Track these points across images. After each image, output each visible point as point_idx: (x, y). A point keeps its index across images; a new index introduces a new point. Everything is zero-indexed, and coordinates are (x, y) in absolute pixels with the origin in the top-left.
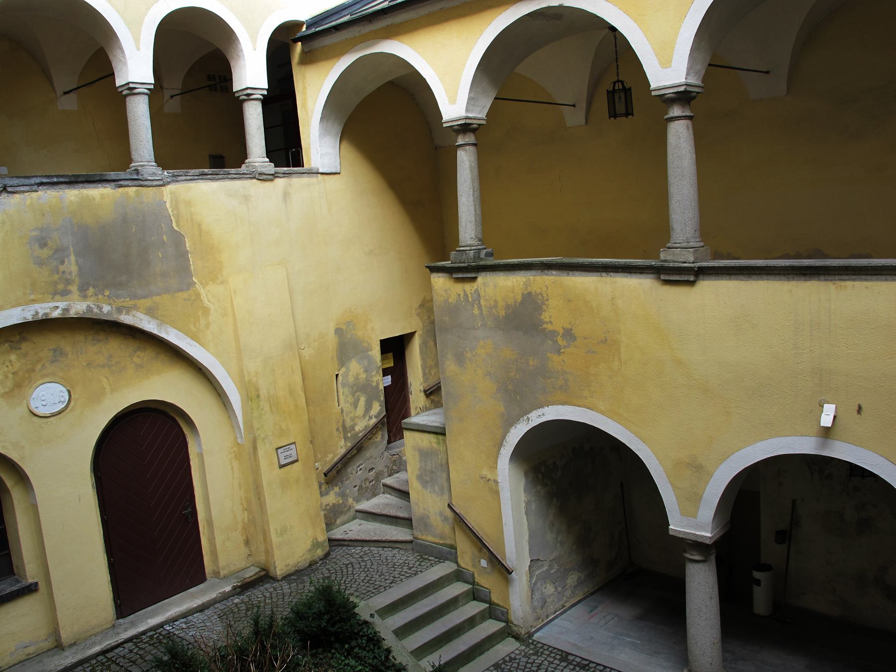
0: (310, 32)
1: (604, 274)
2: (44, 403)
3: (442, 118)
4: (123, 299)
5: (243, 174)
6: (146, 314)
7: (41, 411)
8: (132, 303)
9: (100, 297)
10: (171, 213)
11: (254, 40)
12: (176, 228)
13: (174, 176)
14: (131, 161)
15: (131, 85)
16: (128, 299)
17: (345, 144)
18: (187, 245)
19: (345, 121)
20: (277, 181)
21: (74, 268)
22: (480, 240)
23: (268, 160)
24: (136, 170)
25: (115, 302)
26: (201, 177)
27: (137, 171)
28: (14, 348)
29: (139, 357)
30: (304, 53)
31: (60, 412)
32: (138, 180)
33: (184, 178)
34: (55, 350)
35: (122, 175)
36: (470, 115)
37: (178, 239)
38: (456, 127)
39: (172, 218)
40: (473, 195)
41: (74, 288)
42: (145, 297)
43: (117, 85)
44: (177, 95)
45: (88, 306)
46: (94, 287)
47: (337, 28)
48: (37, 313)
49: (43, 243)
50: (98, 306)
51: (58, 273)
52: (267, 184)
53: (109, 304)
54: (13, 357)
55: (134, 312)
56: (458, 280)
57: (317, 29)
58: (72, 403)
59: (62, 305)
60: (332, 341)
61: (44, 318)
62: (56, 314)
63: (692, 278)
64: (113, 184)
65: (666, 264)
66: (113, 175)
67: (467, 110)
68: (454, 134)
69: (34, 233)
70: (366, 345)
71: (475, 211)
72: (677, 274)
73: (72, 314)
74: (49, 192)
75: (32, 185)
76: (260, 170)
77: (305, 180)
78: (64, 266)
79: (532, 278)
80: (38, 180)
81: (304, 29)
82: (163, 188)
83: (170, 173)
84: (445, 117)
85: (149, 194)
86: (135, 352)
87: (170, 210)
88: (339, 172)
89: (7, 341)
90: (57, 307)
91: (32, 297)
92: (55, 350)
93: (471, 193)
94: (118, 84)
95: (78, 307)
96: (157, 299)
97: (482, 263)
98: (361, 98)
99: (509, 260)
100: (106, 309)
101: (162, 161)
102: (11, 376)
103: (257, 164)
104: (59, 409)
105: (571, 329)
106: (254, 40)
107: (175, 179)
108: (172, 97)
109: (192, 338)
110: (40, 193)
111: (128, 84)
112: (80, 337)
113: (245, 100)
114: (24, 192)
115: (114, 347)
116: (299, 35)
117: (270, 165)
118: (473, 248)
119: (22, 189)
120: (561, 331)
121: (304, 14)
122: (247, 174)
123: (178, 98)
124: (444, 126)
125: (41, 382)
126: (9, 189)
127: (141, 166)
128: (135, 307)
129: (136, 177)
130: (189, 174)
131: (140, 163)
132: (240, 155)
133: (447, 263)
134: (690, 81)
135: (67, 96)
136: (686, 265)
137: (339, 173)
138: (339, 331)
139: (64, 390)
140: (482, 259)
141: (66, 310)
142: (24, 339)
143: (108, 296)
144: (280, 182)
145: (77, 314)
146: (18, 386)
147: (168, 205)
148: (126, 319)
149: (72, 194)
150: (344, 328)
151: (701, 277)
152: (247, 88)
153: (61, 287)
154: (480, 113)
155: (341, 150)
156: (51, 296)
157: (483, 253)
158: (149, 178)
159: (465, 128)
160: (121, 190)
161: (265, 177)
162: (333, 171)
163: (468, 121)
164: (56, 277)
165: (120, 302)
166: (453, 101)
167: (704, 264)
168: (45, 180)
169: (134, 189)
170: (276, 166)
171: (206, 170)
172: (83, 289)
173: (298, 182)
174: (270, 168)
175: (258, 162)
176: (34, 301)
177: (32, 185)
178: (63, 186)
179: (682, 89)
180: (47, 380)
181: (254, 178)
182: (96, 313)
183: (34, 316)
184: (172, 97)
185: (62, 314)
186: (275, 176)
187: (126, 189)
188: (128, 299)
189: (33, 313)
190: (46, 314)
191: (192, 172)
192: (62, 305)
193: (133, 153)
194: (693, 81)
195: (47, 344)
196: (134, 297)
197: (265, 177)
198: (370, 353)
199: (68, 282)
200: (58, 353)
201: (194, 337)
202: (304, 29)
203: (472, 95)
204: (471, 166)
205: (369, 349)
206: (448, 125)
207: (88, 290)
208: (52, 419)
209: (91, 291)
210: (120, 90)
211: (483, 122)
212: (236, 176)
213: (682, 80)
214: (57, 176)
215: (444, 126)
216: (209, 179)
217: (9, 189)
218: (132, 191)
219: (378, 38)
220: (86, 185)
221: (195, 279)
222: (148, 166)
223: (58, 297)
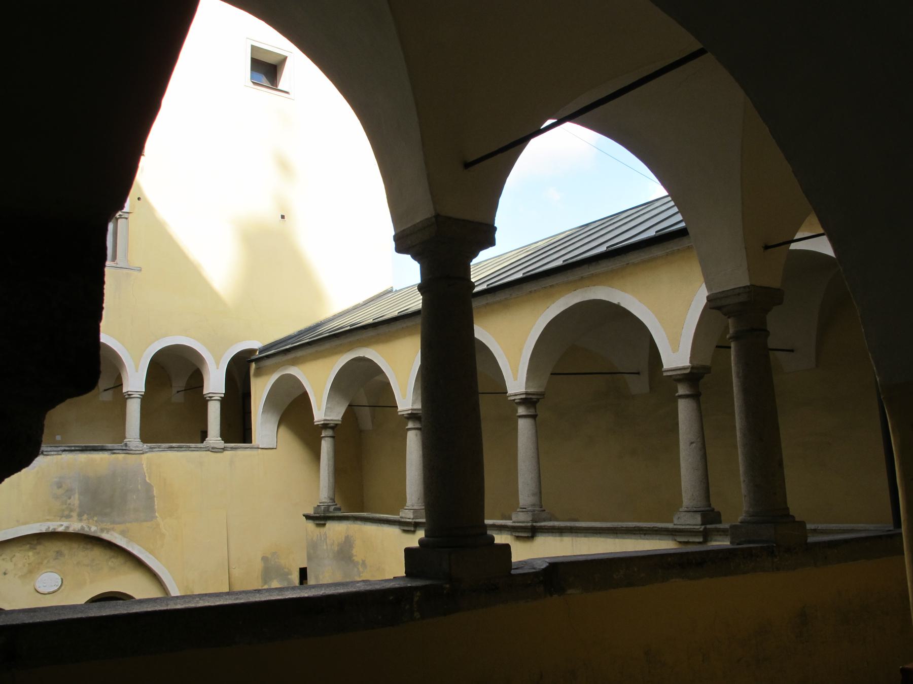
1: (379, 525)
2: (45, 585)
3: (662, 366)
4: (105, 524)
5: (200, 448)
6: (120, 534)
7: (41, 590)
8: (112, 526)
9: (91, 521)
11: (218, 363)
12: (148, 481)
13: (151, 448)
14: (125, 438)
15: (129, 393)
16: (109, 524)
17: (283, 429)
18: (155, 492)
19: (281, 413)
20: (226, 452)
21: (77, 502)
22: (331, 499)
23: (220, 439)
24: (126, 444)
25: (100, 525)
26: (170, 449)
27: (126, 445)
28: (32, 548)
29: (112, 562)
30: (257, 369)
31: (54, 592)
32: (126, 450)
34: (57, 552)
35: (116, 446)
37: (148, 488)
38: (320, 425)
40: (328, 469)
41: (74, 514)
42: (119, 523)
43: (124, 392)
44: (182, 391)
45: (82, 526)
46: (88, 515)
47: (268, 357)
48: (49, 528)
49: (59, 485)
50: (89, 527)
51: (66, 505)
53: (96, 526)
54: (31, 554)
55: (112, 532)
56: (405, 531)
58: (63, 587)
59: (65, 524)
60: (258, 565)
61: (53, 531)
62: (61, 529)
63: (412, 529)
64: (109, 452)
65: (403, 520)
66: (109, 446)
67: (325, 415)
68: (515, 405)
69: (55, 480)
70: (286, 570)
71: (329, 480)
72: (522, 532)
73: (71, 530)
74: (68, 455)
75: (59, 451)
76: (212, 445)
77: (254, 452)
78: (71, 500)
79: (349, 525)
80: (63, 448)
81: (257, 353)
84: (666, 366)
86: (111, 558)
87: (145, 469)
89: (28, 543)
90: (62, 525)
91: (48, 518)
92: (57, 552)
93: (327, 469)
94: (124, 391)
95: (75, 526)
96: (128, 525)
97: (331, 515)
98: (291, 400)
99: (382, 515)
100: (93, 529)
101: (147, 436)
102: (27, 565)
104: (54, 589)
105: (365, 560)
106: (218, 363)
108: (178, 392)
109: (150, 553)
111: (128, 392)
112: (75, 545)
114: (53, 455)
115: (97, 553)
116: (253, 357)
119: (52, 453)
120: (361, 562)
121: (256, 344)
122: (204, 448)
123: (183, 392)
125: (45, 571)
126: (45, 453)
127: (129, 441)
128: (113, 529)
132: (204, 435)
134: (529, 391)
135: (106, 392)
138: (264, 559)
139: (60, 578)
140: (331, 512)
141: (68, 527)
142: (39, 543)
143: (96, 521)
144: (228, 453)
145: (74, 530)
146: (30, 572)
147: (144, 466)
148: (106, 536)
149: (83, 457)
150: (270, 556)
151: (418, 528)
153: (66, 513)
155: (278, 434)
156: (59, 518)
157: (332, 508)
158: (134, 449)
159: (325, 426)
161: (217, 450)
162: (271, 447)
163: (326, 422)
164: (64, 507)
165: (103, 526)
166: (675, 347)
168: (67, 448)
169: (123, 455)
170: (225, 443)
171: (174, 445)
172: (80, 515)
174: (221, 444)
176: (48, 520)
177: (59, 451)
178: (78, 452)
179: (410, 412)
180: (49, 570)
181: (209, 450)
182: (87, 531)
183: (47, 529)
184: (178, 392)
185: (65, 529)
186: (224, 449)
187: (118, 455)
188: (109, 524)
189: (47, 527)
190: (54, 529)
192: (65, 524)
193: (127, 433)
195: (51, 548)
196: (114, 522)
197: (217, 450)
198: (290, 577)
199: (71, 510)
200: (59, 554)
201: (152, 552)
202: (257, 353)
203: (329, 405)
204: (328, 450)
205: (289, 573)
207: (83, 516)
208: (48, 596)
209: (85, 517)
210: (125, 394)
211: (340, 422)
212: (195, 449)
213: (523, 390)
214: (74, 446)
216: (175, 451)
217: (45, 453)
218: (121, 456)
219: (289, 365)
220: (92, 452)
221: (157, 514)
223: (64, 519)
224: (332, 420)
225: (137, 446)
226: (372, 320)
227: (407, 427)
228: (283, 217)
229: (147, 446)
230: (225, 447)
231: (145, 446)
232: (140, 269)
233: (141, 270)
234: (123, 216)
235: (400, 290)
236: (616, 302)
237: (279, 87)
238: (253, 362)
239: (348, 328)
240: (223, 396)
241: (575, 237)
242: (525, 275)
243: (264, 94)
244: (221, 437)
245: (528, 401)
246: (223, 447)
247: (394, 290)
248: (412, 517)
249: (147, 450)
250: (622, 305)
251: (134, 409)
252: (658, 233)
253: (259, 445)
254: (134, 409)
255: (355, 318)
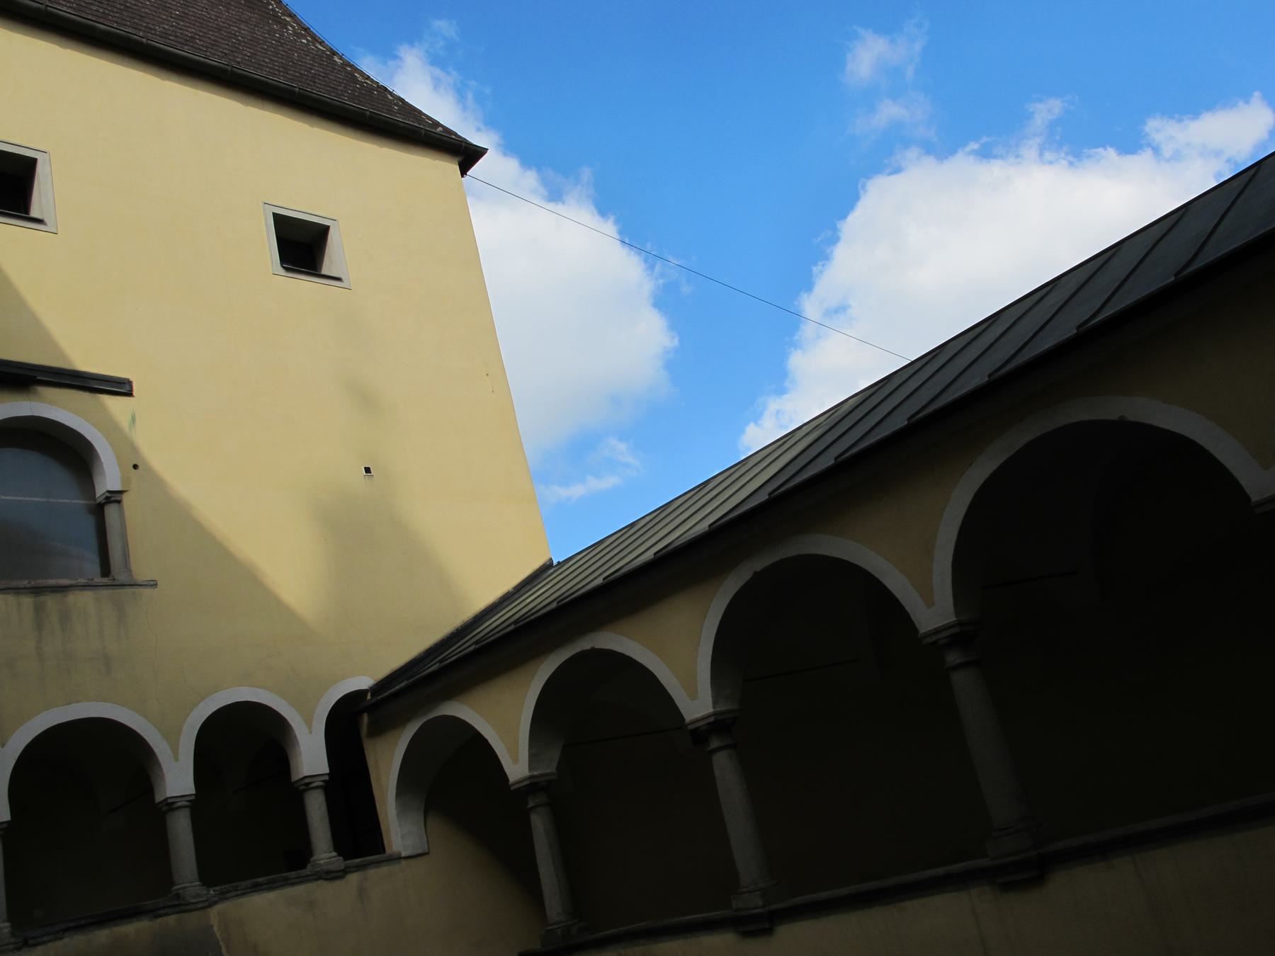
0: (374, 700)
5: (306, 876)
10: (219, 938)
11: (309, 722)
14: (172, 884)
15: (170, 801)
23: (335, 854)
27: (178, 896)
32: (181, 905)
33: (234, 893)
36: (535, 773)
39: (221, 943)
47: (396, 695)
52: (337, 883)
57: (379, 698)
67: (531, 768)
77: (395, 867)
81: (369, 697)
82: (209, 910)
83: (217, 891)
84: (512, 778)
85: (192, 920)
87: (218, 934)
88: (427, 851)
99: (688, 917)
101: (208, 875)
103: (322, 862)
106: (309, 722)
107: (223, 897)
110: (66, 940)
113: (305, 791)
117: (338, 860)
118: (560, 925)
119: (45, 939)
121: (364, 682)
124: (512, 789)
126: (31, 942)
127: (184, 888)
129: (177, 903)
130: (240, 888)
131: (182, 886)
133: (984, 862)
136: (756, 911)
137: (428, 854)
144: (353, 878)
147: (215, 929)
152: (306, 777)
154: (549, 767)
158: (193, 901)
160: (159, 920)
161: (334, 875)
162: (420, 851)
163: (534, 780)
166: (693, 694)
167: (774, 907)
168: (72, 924)
170: (345, 859)
171: (260, 880)
173: (375, 874)
174: (337, 862)
175: (323, 859)
179: (712, 719)
187: (165, 918)
191: (243, 884)
194: (722, 708)
197: (334, 875)
202: (369, 697)
206: (930, 640)
213: (711, 710)
215: (512, 789)
218: (171, 920)
222: (191, 887)
224: (541, 775)
225: (198, 895)
226: (555, 603)
227: (709, 749)
228: (368, 470)
229: (214, 891)
230: (346, 868)
231: (212, 892)
232: (155, 583)
233: (156, 585)
234: (113, 499)
235: (565, 561)
236: (1115, 417)
237: (324, 271)
238: (364, 712)
239: (512, 627)
240: (327, 778)
241: (566, 570)
242: (560, 604)
243: (303, 285)
244: (335, 851)
245: (959, 636)
246: (343, 868)
247: (555, 562)
248: (760, 903)
249: (216, 899)
250: (1130, 418)
251: (181, 828)
252: (1081, 329)
253: (400, 853)
254: (181, 828)
255: (510, 610)
